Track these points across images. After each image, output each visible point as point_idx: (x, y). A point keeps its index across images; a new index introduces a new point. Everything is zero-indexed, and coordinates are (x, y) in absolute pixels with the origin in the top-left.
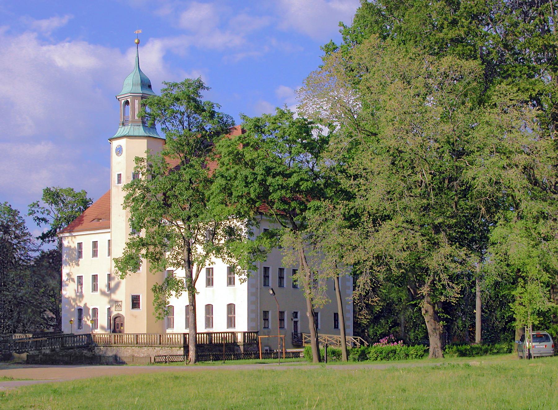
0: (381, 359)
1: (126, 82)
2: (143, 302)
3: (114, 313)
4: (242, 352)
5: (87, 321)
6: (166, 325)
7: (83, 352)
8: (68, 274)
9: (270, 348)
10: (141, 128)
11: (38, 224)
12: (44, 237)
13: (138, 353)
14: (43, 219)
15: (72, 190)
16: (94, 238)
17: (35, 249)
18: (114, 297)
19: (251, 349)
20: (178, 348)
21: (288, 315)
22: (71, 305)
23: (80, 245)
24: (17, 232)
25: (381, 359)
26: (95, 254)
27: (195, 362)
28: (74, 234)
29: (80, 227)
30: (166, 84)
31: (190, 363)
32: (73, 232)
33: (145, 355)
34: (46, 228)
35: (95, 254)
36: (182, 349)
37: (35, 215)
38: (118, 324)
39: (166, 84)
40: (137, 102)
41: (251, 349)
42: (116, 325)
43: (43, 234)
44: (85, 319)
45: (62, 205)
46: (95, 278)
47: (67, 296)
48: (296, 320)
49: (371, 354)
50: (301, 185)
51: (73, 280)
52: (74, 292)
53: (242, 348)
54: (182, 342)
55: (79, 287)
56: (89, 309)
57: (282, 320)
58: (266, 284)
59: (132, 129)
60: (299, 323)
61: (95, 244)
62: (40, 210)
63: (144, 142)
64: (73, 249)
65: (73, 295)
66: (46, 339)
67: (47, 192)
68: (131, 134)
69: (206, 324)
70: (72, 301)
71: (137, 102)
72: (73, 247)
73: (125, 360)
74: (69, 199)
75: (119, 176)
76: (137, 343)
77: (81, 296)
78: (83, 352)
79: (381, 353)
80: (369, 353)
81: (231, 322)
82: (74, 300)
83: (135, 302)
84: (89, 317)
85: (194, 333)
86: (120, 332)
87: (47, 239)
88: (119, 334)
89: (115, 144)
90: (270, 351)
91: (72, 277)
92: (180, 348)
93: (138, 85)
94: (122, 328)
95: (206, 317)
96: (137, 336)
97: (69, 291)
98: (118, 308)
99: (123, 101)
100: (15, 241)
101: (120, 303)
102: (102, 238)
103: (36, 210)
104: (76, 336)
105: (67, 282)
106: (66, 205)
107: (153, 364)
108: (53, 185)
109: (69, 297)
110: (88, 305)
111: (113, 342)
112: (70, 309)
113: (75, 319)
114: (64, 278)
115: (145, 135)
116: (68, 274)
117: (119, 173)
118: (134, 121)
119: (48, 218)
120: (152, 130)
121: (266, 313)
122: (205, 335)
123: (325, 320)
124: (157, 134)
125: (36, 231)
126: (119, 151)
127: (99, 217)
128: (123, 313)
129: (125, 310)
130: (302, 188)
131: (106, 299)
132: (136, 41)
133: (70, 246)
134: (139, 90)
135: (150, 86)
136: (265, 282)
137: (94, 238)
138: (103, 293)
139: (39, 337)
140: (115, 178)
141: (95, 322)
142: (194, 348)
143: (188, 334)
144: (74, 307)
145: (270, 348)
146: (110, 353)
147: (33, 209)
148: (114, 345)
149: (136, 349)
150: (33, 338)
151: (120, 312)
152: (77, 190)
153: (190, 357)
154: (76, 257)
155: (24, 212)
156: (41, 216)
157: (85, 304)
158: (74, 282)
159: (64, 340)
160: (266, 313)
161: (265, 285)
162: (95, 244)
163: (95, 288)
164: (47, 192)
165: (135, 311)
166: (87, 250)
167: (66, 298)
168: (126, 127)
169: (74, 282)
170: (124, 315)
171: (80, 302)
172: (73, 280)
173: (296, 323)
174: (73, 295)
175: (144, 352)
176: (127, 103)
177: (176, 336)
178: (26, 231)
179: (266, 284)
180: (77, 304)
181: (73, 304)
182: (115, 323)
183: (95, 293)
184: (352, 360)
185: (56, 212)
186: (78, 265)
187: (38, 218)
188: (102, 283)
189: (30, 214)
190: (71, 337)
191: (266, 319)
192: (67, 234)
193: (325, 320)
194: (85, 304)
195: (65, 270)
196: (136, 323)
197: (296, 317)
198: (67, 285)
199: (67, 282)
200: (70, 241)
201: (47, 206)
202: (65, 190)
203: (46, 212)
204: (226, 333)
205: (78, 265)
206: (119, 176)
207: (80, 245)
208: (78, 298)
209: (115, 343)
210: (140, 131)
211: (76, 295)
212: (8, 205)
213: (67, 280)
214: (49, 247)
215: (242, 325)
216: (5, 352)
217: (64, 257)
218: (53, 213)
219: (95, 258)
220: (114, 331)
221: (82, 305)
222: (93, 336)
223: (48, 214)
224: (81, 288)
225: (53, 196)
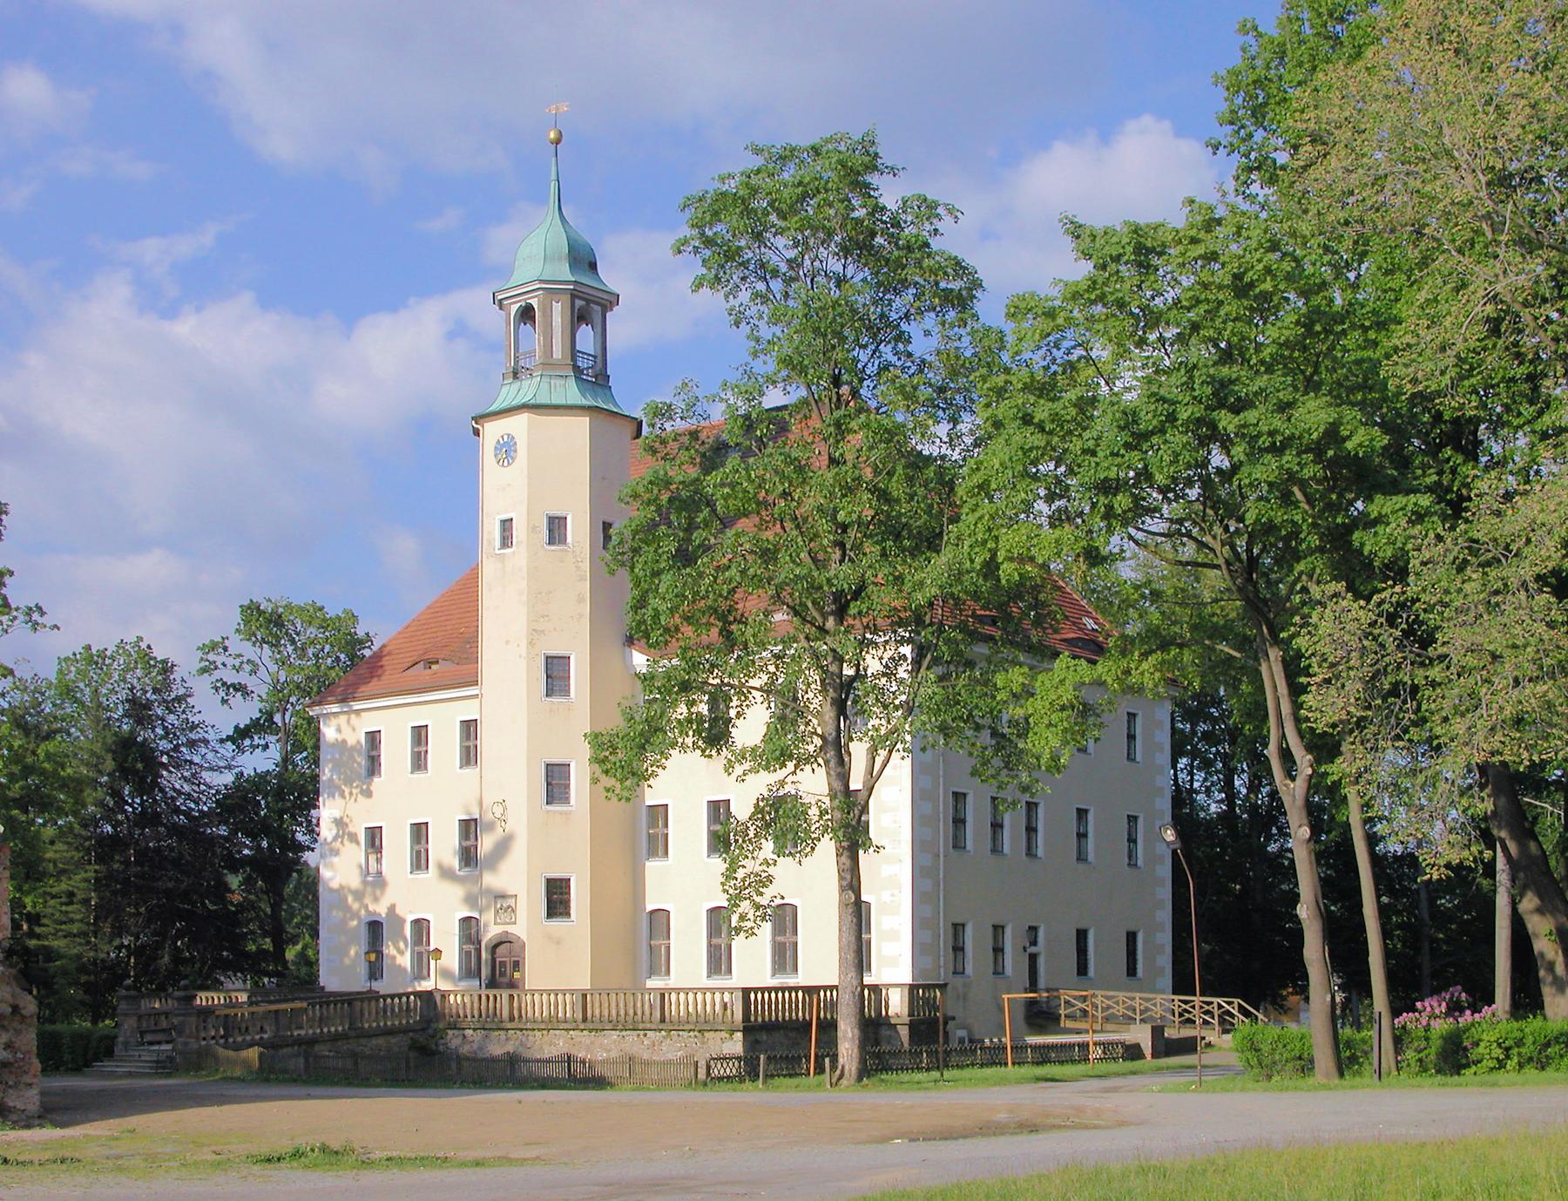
0: (1521, 1065)
1: (524, 251)
2: (579, 897)
3: (491, 931)
4: (906, 1045)
5: (400, 956)
6: (645, 966)
7: (415, 1048)
8: (339, 823)
9: (970, 1032)
10: (572, 382)
11: (224, 701)
12: (241, 735)
13: (588, 1049)
14: (240, 688)
15: (321, 609)
16: (419, 716)
17: (221, 764)
18: (490, 880)
19: (928, 1038)
20: (724, 1035)
21: (1014, 937)
22: (348, 908)
23: (373, 738)
24: (171, 718)
25: (1521, 1065)
26: (419, 762)
27: (860, 1079)
28: (357, 706)
29: (374, 685)
30: (758, 151)
31: (844, 1082)
32: (354, 699)
33: (614, 1054)
34: (245, 712)
35: (419, 762)
36: (739, 1035)
37: (217, 674)
38: (503, 964)
39: (758, 151)
40: (557, 307)
41: (928, 1038)
42: (495, 965)
43: (237, 727)
44: (389, 950)
45: (290, 649)
46: (420, 832)
47: (334, 885)
48: (1033, 950)
49: (1481, 1049)
50: (1349, 437)
51: (353, 838)
52: (357, 871)
53: (904, 1032)
54: (739, 1015)
55: (372, 858)
56: (404, 921)
57: (998, 950)
58: (958, 843)
59: (544, 386)
60: (1041, 961)
61: (420, 734)
62: (230, 661)
63: (583, 423)
64: (353, 748)
65: (355, 881)
66: (305, 1004)
67: (252, 611)
68: (543, 399)
69: (774, 962)
70: (350, 899)
71: (557, 307)
72: (351, 741)
73: (607, 1072)
74: (312, 632)
75: (507, 525)
76: (585, 1019)
77: (376, 882)
78: (415, 1048)
79: (1520, 1043)
80: (1477, 1044)
81: (859, 954)
82: (359, 896)
83: (557, 898)
84: (402, 945)
85: (855, 983)
86: (512, 985)
87: (247, 742)
88: (505, 994)
89: (493, 431)
90: (971, 1041)
91: (351, 829)
92: (732, 1032)
93: (560, 259)
94: (517, 975)
95: (710, 945)
96: (584, 996)
97: (338, 870)
98: (504, 916)
99: (514, 308)
100: (164, 745)
101: (511, 902)
102: (443, 715)
103: (219, 660)
104: (385, 997)
105: (337, 845)
106: (302, 651)
107: (705, 1084)
108: (269, 595)
109: (342, 887)
110: (399, 911)
111: (506, 1014)
112: (344, 922)
113: (356, 951)
114: (326, 831)
115: (585, 402)
116: (339, 823)
117: (507, 516)
118: (548, 364)
119: (250, 682)
120: (600, 390)
121: (958, 929)
122: (800, 994)
123: (1105, 952)
124: (616, 405)
125: (218, 716)
126: (506, 450)
127: (430, 656)
128: (519, 930)
129: (526, 922)
130: (1349, 445)
131: (456, 892)
132: (552, 135)
133: (344, 741)
134: (564, 272)
135: (593, 266)
136: (955, 837)
137: (419, 716)
138: (446, 873)
139: (286, 1001)
140: (492, 531)
141: (424, 956)
142: (856, 1031)
143: (836, 987)
144: (356, 915)
145: (970, 1032)
146: (498, 1046)
147: (211, 657)
148: (509, 1025)
149: (583, 1037)
150: (251, 1003)
151: (511, 929)
152: (332, 611)
153: (841, 1060)
154: (363, 772)
155: (186, 665)
156: (231, 677)
157: (392, 908)
158: (358, 843)
159: (358, 1009)
160: (958, 929)
161: (954, 847)
162: (420, 734)
163: (420, 861)
164: (252, 611)
165: (557, 924)
166: (396, 751)
167: (331, 890)
168: (526, 383)
169: (358, 843)
170: (524, 937)
171: (376, 900)
172: (353, 838)
173: (1033, 958)
174: (355, 881)
175: (672, 1048)
176: (527, 314)
177: (682, 996)
178: (196, 719)
179: (958, 843)
180: (366, 907)
181: (356, 906)
182: (494, 960)
183: (421, 876)
184: (1415, 1067)
185: (273, 668)
186: (368, 794)
187: (224, 684)
188: (445, 845)
189: (204, 670)
190: (370, 999)
191: (958, 949)
192: (335, 708)
193: (1105, 952)
194: (392, 908)
195: (328, 811)
196: (558, 963)
197: (1034, 943)
198: (337, 853)
199: (337, 845)
200: (341, 727)
201: (249, 651)
202: (301, 609)
203: (248, 668)
204: (769, 990)
205: (368, 794)
206: (507, 525)
207: (373, 738)
208: (369, 889)
209: (512, 1019)
210: (571, 393)
211: (365, 883)
212: (143, 645)
213: (335, 839)
214: (261, 760)
215: (894, 964)
216: (186, 1044)
217: (326, 773)
218: (264, 669)
219: (419, 776)
220: (492, 983)
221: (380, 909)
222: (438, 999)
223: (254, 672)
224: (379, 861)
225: (267, 623)
